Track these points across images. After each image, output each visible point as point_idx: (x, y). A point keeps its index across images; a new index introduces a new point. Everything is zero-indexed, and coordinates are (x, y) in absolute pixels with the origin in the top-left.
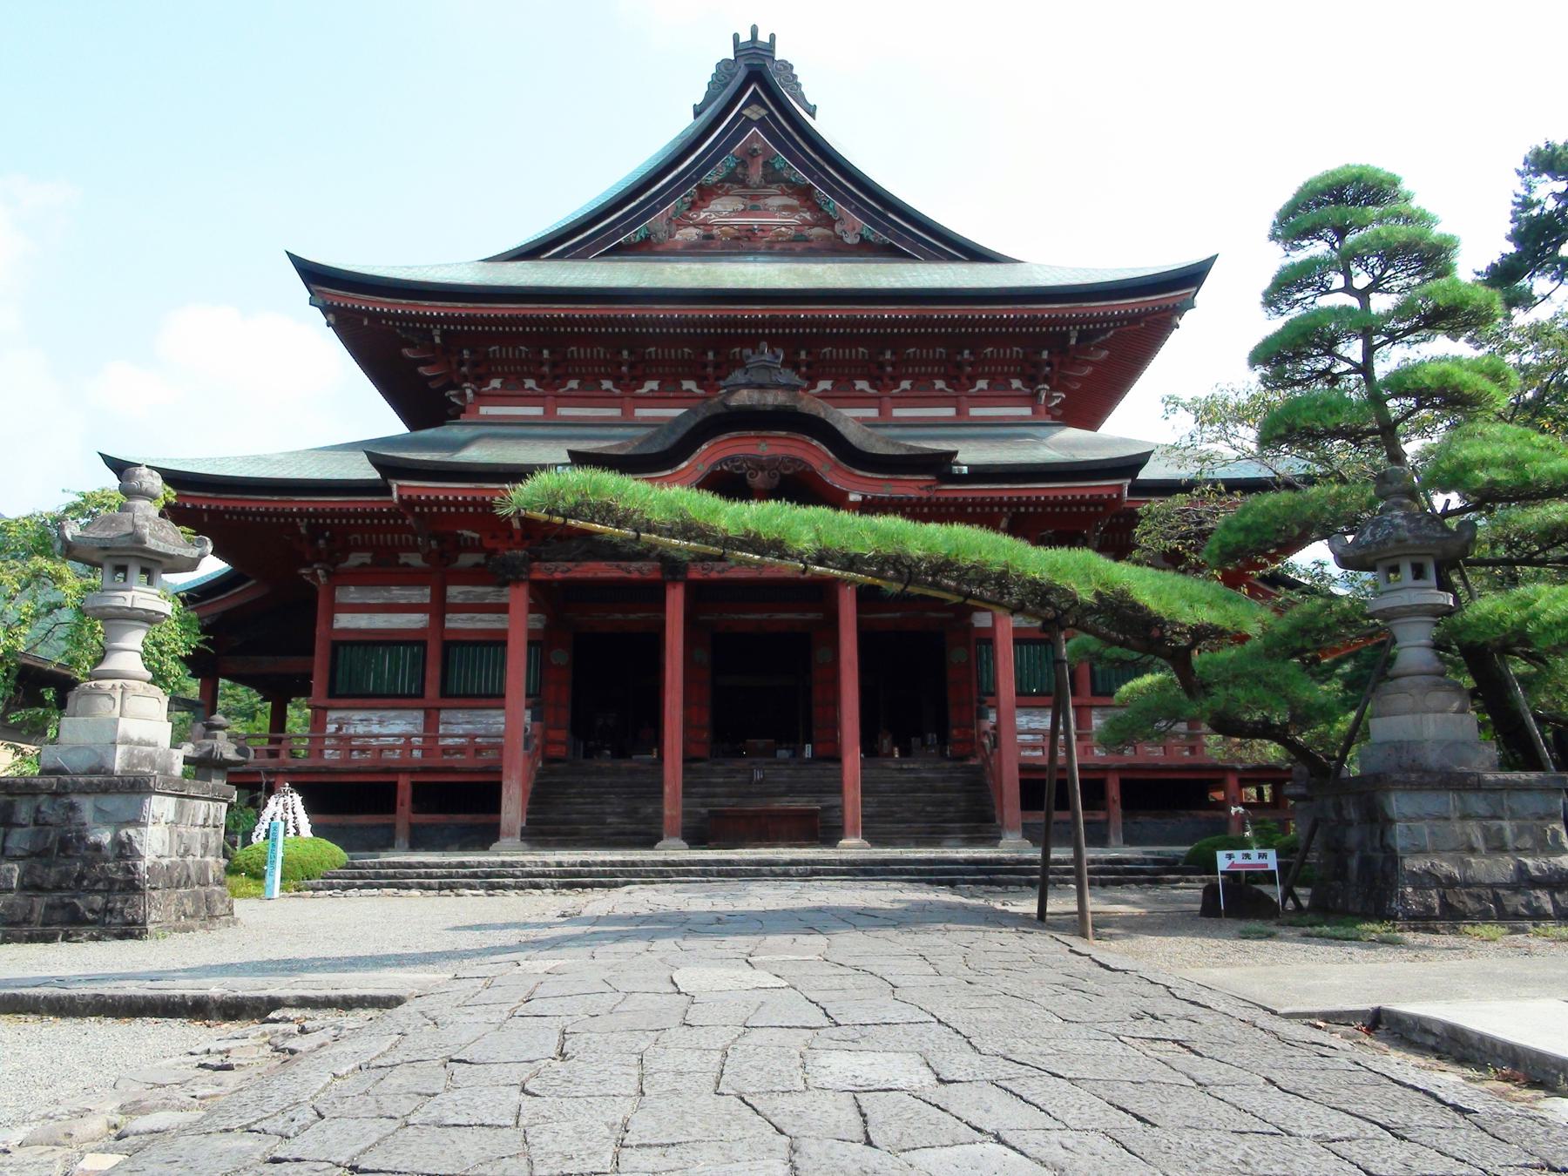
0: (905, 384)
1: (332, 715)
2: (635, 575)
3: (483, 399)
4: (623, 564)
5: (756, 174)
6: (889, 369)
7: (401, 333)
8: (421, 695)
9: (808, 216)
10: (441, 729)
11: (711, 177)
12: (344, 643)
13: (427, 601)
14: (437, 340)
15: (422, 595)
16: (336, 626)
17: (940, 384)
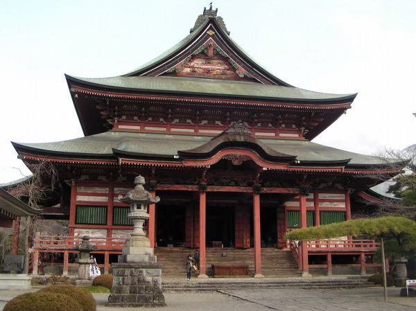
0: (259, 125)
1: (76, 230)
2: (190, 190)
3: (120, 123)
4: (187, 186)
5: (211, 53)
6: (170, 116)
7: (95, 104)
8: (106, 224)
9: (226, 66)
10: (113, 235)
11: (196, 52)
12: (80, 206)
13: (108, 192)
14: (108, 103)
15: (106, 190)
16: (77, 200)
17: (270, 125)
